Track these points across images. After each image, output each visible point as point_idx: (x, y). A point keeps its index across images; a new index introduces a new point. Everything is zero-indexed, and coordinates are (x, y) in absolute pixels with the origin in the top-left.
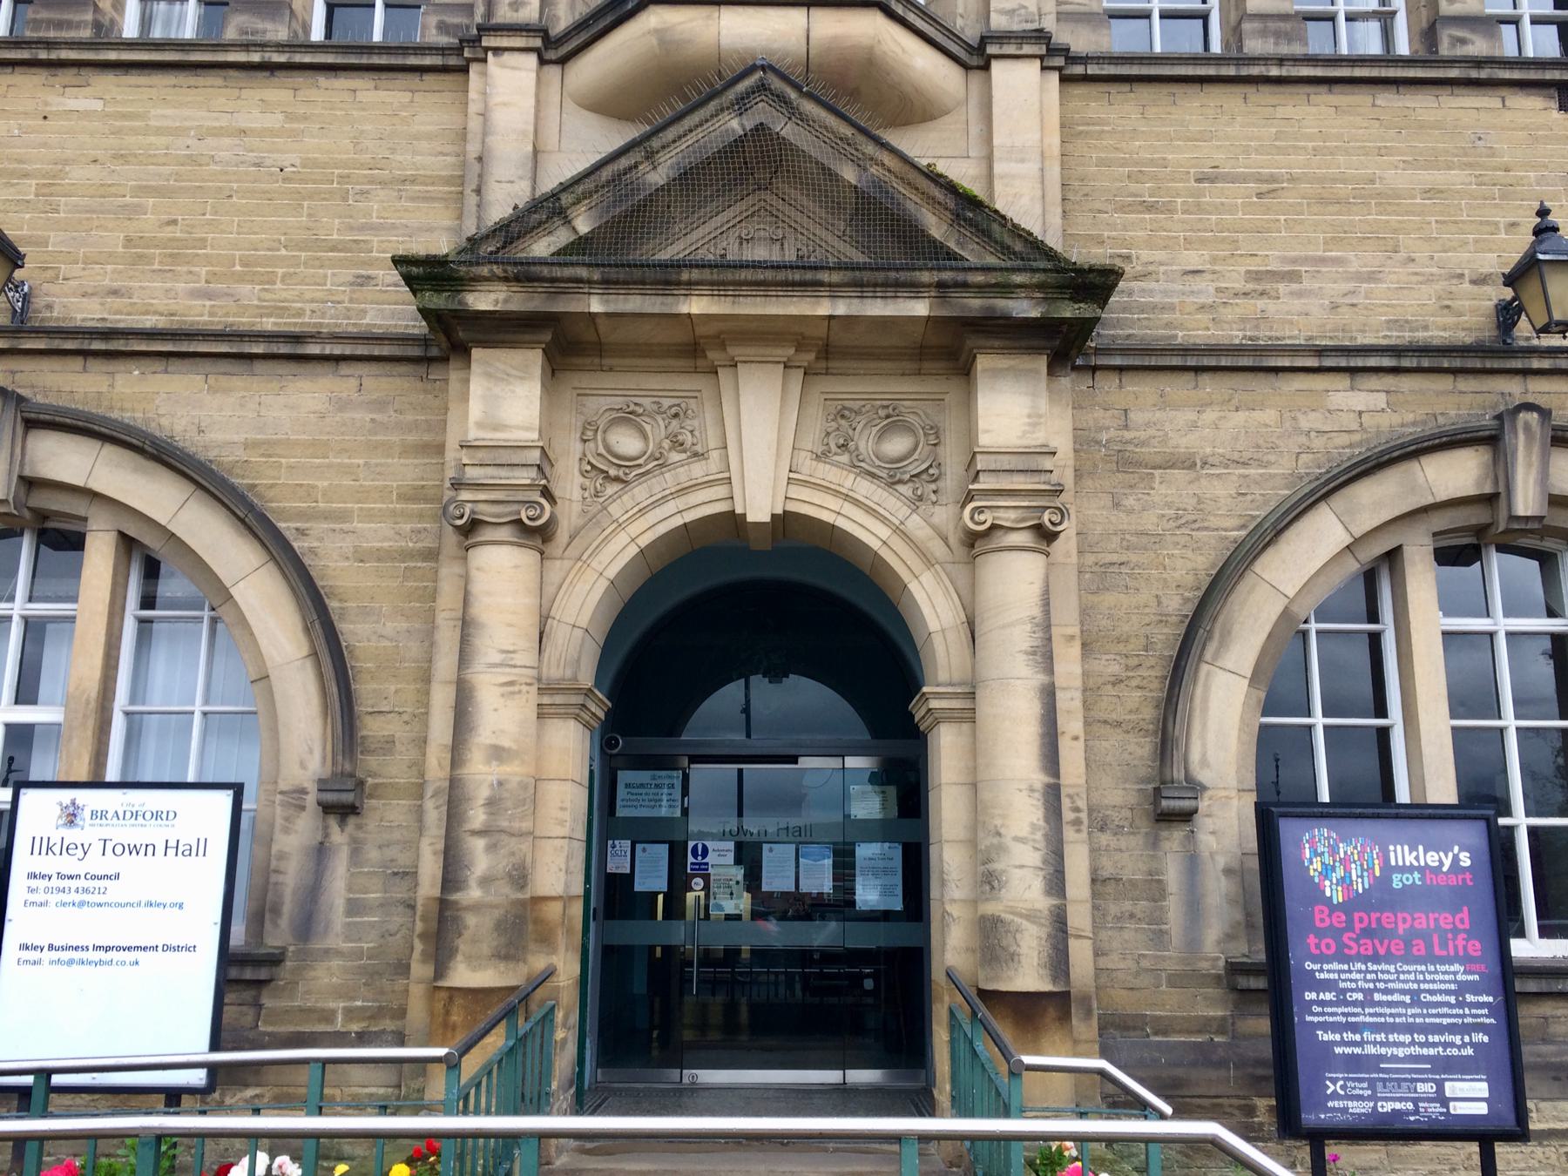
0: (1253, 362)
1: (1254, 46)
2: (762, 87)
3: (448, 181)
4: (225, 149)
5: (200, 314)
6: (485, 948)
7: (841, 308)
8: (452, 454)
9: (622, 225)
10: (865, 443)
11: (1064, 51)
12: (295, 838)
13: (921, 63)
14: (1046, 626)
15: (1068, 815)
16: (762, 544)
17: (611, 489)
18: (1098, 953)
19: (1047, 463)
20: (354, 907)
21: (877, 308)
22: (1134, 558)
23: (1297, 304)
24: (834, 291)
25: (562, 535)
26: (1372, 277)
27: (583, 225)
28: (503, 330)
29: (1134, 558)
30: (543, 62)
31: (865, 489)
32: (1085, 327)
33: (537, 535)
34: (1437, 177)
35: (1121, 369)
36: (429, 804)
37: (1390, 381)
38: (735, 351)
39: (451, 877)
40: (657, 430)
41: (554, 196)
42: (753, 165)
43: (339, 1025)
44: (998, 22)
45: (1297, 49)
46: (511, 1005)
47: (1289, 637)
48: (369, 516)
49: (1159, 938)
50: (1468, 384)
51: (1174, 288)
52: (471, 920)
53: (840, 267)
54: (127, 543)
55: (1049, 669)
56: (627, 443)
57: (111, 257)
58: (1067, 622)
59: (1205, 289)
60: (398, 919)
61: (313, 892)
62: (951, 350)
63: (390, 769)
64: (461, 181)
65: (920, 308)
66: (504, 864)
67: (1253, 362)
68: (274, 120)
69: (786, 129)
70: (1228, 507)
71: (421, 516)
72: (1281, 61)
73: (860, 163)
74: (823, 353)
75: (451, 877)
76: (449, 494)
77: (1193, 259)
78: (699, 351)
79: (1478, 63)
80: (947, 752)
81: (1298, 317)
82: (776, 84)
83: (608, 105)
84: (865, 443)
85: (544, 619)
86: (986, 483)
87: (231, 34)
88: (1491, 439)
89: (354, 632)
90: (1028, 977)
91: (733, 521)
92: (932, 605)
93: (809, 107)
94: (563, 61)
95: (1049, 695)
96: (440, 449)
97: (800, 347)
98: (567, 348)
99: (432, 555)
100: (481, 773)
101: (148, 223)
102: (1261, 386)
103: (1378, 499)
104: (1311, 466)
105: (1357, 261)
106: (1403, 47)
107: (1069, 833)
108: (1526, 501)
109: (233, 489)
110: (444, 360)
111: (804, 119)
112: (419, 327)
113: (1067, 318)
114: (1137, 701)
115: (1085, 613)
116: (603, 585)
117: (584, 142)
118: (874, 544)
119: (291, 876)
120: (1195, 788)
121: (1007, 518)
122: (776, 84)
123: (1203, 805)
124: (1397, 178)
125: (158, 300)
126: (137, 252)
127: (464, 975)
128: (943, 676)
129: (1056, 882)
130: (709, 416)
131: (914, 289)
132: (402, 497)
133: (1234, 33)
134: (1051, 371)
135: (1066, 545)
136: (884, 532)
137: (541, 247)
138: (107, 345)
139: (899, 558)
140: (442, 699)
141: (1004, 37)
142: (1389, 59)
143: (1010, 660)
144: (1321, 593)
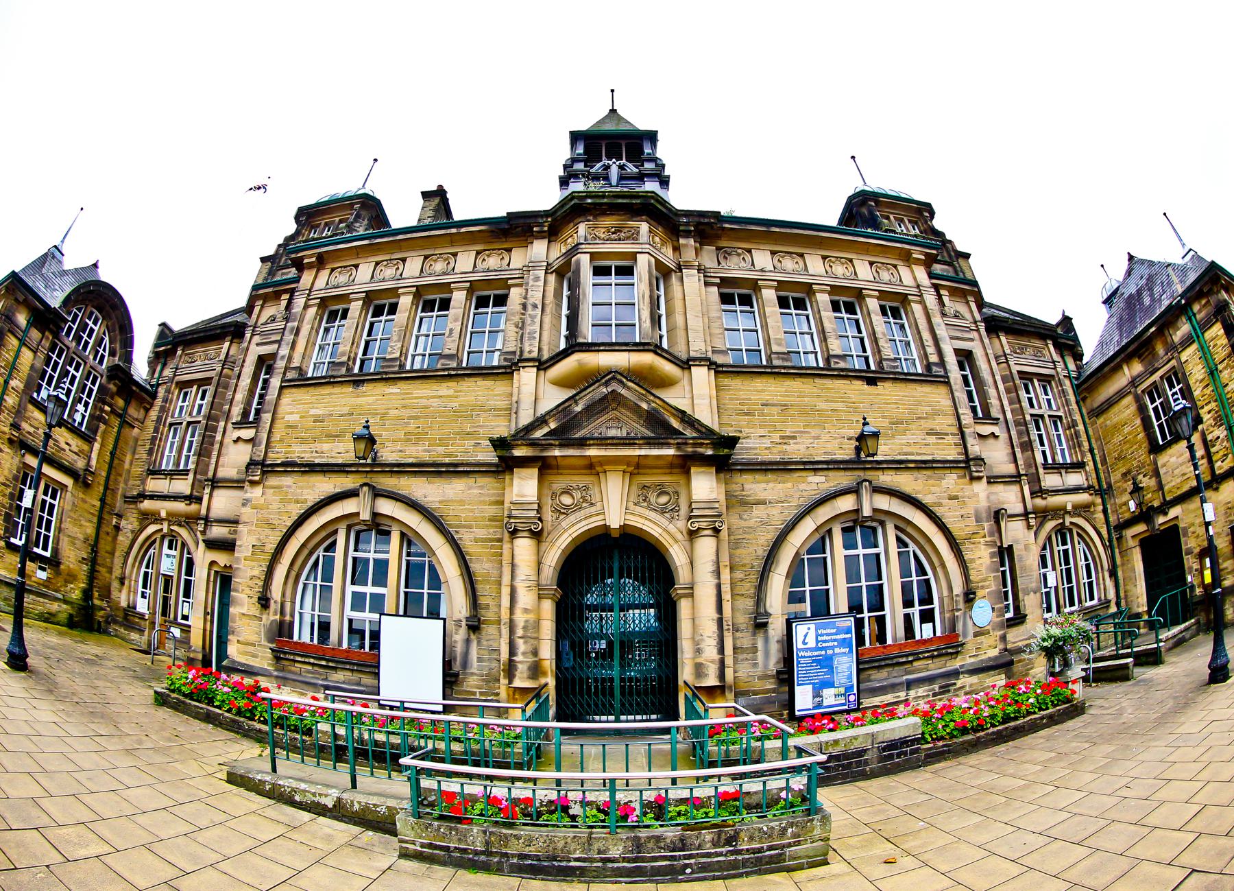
0: (782, 468)
1: (776, 362)
2: (614, 378)
3: (506, 409)
4: (435, 403)
5: (426, 457)
6: (525, 675)
7: (643, 452)
8: (507, 505)
9: (566, 425)
10: (652, 497)
11: (715, 363)
12: (459, 636)
13: (668, 368)
14: (718, 562)
15: (725, 627)
16: (615, 535)
17: (562, 517)
18: (735, 672)
19: (717, 505)
20: (480, 660)
21: (643, 452)
22: (747, 536)
23: (796, 447)
24: (640, 446)
25: (545, 534)
26: (818, 438)
27: (553, 425)
28: (524, 462)
29: (747, 536)
30: (539, 369)
31: (652, 515)
32: (728, 457)
33: (537, 535)
34: (835, 405)
35: (741, 470)
36: (503, 627)
37: (826, 473)
38: (606, 467)
39: (512, 651)
40: (577, 495)
41: (543, 416)
42: (610, 402)
43: (478, 697)
44: (693, 354)
45: (789, 364)
46: (537, 693)
47: (797, 562)
48: (478, 527)
49: (755, 665)
50: (849, 473)
51: (756, 444)
52: (520, 666)
53: (642, 438)
54: (403, 535)
55: (719, 578)
56: (567, 500)
57: (400, 440)
58: (725, 560)
59: (766, 442)
60: (495, 664)
61: (466, 654)
62: (684, 465)
63: (489, 614)
64: (510, 409)
65: (671, 452)
66: (530, 649)
67: (782, 468)
68: (451, 392)
69: (623, 392)
70: (779, 516)
71: (496, 527)
72: (784, 367)
73: (648, 403)
74: (637, 467)
75: (512, 651)
76: (506, 520)
77: (762, 432)
78: (592, 468)
79: (843, 370)
80: (684, 607)
81: (796, 451)
82: (619, 377)
83: (561, 383)
84: (652, 497)
85: (539, 563)
86: (696, 513)
87: (439, 366)
88: (855, 490)
89: (475, 567)
90: (712, 681)
91: (606, 527)
92: (677, 555)
93: (630, 384)
94: (545, 369)
95: (719, 587)
96: (502, 503)
97: (628, 465)
98: (545, 467)
99: (500, 540)
100: (520, 618)
101: (411, 428)
102: (787, 476)
103: (824, 513)
104: (805, 503)
105: (814, 432)
106: (821, 365)
107: (726, 633)
108: (867, 512)
109: (435, 517)
110: (503, 472)
111: (629, 388)
112: (496, 460)
113: (721, 454)
114: (748, 587)
115: (731, 557)
116: (560, 551)
117: (553, 397)
118: (657, 535)
119: (459, 649)
120: (768, 615)
121: (703, 525)
122: (619, 377)
123: (770, 620)
124: (823, 405)
125: (416, 453)
126: (408, 437)
127: (518, 683)
128: (682, 581)
129: (721, 650)
130: (597, 490)
131: (668, 445)
132: (490, 520)
133: (769, 359)
134: (717, 472)
135: (724, 534)
136: (660, 531)
137: (538, 434)
138: (399, 469)
139: (665, 540)
140: (506, 591)
141: (695, 359)
142: (818, 368)
143: (697, 566)
144: (808, 546)
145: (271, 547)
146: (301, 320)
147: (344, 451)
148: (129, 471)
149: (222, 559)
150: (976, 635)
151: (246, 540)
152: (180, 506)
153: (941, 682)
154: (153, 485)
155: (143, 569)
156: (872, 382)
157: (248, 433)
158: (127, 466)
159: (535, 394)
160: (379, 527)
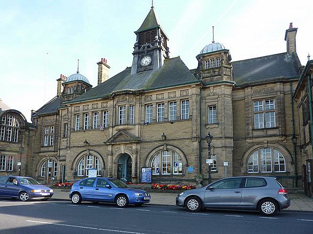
81: (154, 139)
145: (73, 161)
146: (71, 118)
147: (82, 144)
148: (34, 147)
149: (63, 163)
150: (189, 173)
151: (68, 160)
152: (53, 153)
153: (179, 181)
154: (42, 149)
155: (42, 167)
156: (172, 123)
157: (65, 139)
158: (33, 146)
159: (112, 132)
160: (90, 154)
